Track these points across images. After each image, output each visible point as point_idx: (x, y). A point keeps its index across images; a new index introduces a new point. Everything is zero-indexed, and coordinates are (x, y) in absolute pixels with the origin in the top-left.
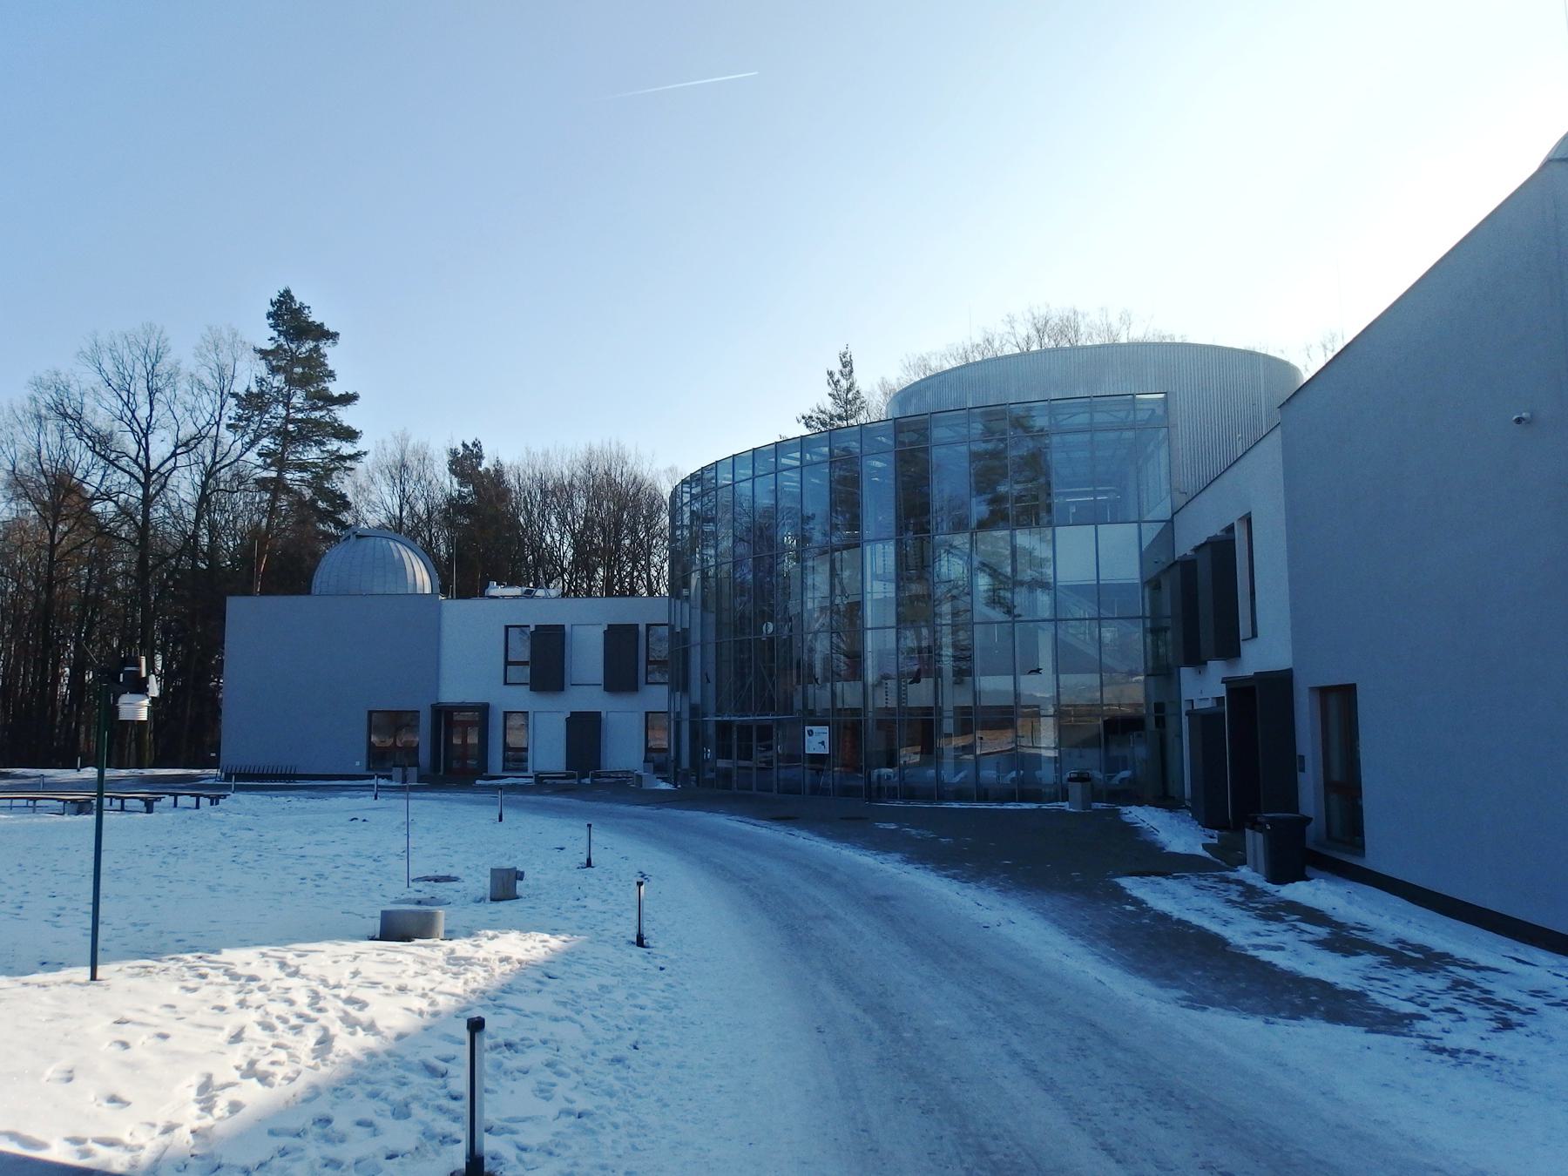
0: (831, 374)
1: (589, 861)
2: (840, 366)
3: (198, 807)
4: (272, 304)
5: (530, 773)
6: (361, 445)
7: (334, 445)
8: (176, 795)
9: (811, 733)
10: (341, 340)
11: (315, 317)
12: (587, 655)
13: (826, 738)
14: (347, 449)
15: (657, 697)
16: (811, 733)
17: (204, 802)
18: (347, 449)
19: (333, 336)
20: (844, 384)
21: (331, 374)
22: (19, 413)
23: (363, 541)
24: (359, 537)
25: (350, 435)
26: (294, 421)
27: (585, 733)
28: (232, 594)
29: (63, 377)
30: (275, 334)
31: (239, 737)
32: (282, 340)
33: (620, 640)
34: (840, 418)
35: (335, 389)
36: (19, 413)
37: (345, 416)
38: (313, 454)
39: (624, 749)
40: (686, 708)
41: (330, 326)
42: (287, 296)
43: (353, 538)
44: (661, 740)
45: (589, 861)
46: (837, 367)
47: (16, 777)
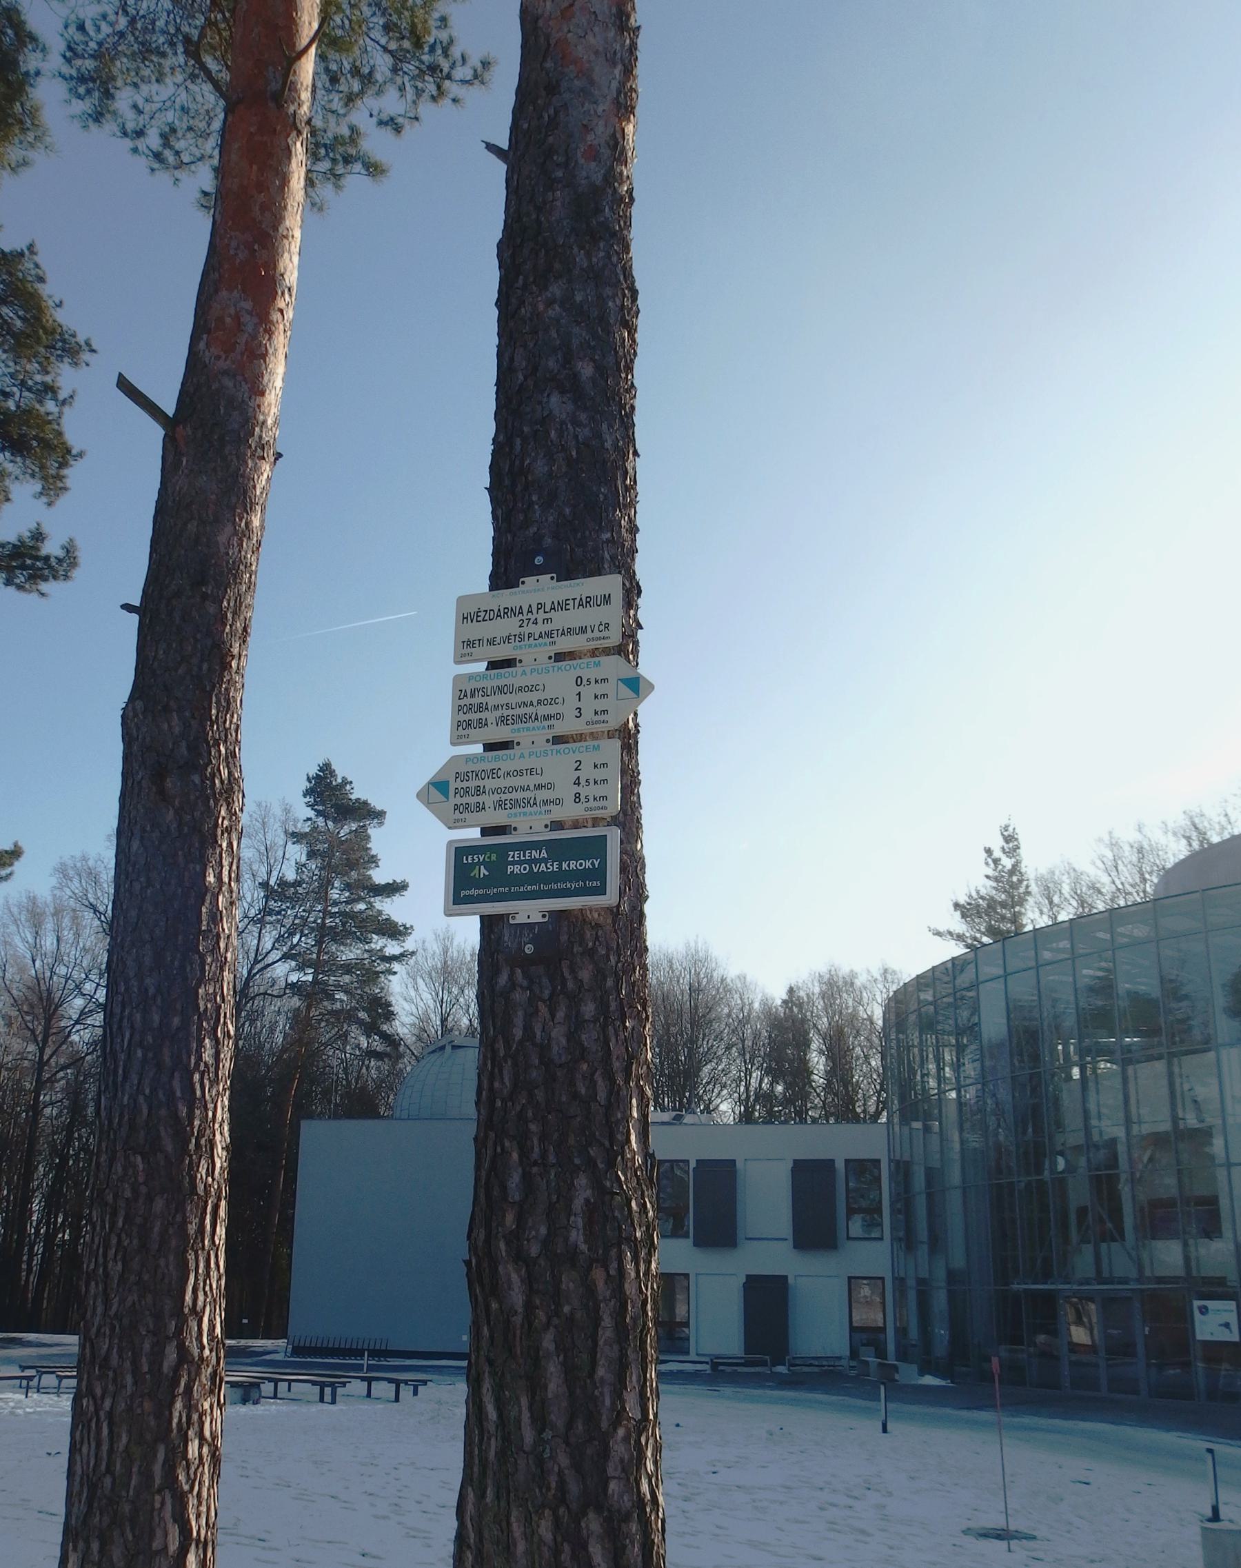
0: (989, 851)
1: (1215, 1509)
2: (1001, 842)
3: (397, 1399)
4: (309, 780)
5: (693, 1357)
6: (410, 944)
7: (378, 942)
8: (369, 1381)
9: (1204, 1310)
10: (388, 819)
11: (358, 792)
12: (767, 1201)
13: (1233, 1319)
14: (393, 948)
15: (872, 1256)
16: (1204, 1310)
17: (406, 1391)
18: (393, 948)
19: (379, 815)
20: (1007, 863)
21: (374, 860)
22: (15, 910)
23: (461, 1052)
24: (454, 1047)
25: (394, 931)
26: (333, 915)
27: (767, 1302)
28: (304, 1118)
29: (91, 863)
30: (312, 814)
31: (312, 1303)
32: (320, 821)
33: (810, 1178)
34: (1003, 905)
35: (380, 876)
36: (15, 910)
37: (391, 908)
38: (350, 953)
39: (821, 1327)
40: (941, 1274)
41: (376, 803)
42: (326, 769)
43: (448, 1048)
44: (870, 1316)
45: (1215, 1509)
46: (997, 844)
47: (29, 1344)
